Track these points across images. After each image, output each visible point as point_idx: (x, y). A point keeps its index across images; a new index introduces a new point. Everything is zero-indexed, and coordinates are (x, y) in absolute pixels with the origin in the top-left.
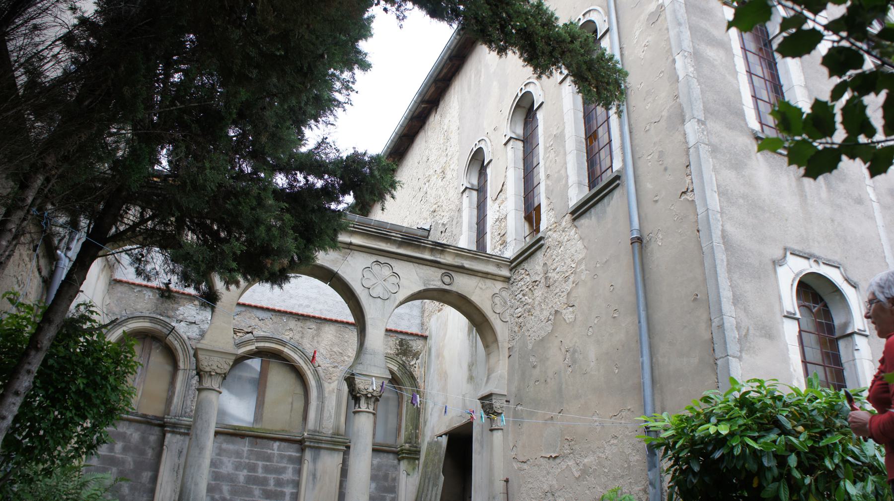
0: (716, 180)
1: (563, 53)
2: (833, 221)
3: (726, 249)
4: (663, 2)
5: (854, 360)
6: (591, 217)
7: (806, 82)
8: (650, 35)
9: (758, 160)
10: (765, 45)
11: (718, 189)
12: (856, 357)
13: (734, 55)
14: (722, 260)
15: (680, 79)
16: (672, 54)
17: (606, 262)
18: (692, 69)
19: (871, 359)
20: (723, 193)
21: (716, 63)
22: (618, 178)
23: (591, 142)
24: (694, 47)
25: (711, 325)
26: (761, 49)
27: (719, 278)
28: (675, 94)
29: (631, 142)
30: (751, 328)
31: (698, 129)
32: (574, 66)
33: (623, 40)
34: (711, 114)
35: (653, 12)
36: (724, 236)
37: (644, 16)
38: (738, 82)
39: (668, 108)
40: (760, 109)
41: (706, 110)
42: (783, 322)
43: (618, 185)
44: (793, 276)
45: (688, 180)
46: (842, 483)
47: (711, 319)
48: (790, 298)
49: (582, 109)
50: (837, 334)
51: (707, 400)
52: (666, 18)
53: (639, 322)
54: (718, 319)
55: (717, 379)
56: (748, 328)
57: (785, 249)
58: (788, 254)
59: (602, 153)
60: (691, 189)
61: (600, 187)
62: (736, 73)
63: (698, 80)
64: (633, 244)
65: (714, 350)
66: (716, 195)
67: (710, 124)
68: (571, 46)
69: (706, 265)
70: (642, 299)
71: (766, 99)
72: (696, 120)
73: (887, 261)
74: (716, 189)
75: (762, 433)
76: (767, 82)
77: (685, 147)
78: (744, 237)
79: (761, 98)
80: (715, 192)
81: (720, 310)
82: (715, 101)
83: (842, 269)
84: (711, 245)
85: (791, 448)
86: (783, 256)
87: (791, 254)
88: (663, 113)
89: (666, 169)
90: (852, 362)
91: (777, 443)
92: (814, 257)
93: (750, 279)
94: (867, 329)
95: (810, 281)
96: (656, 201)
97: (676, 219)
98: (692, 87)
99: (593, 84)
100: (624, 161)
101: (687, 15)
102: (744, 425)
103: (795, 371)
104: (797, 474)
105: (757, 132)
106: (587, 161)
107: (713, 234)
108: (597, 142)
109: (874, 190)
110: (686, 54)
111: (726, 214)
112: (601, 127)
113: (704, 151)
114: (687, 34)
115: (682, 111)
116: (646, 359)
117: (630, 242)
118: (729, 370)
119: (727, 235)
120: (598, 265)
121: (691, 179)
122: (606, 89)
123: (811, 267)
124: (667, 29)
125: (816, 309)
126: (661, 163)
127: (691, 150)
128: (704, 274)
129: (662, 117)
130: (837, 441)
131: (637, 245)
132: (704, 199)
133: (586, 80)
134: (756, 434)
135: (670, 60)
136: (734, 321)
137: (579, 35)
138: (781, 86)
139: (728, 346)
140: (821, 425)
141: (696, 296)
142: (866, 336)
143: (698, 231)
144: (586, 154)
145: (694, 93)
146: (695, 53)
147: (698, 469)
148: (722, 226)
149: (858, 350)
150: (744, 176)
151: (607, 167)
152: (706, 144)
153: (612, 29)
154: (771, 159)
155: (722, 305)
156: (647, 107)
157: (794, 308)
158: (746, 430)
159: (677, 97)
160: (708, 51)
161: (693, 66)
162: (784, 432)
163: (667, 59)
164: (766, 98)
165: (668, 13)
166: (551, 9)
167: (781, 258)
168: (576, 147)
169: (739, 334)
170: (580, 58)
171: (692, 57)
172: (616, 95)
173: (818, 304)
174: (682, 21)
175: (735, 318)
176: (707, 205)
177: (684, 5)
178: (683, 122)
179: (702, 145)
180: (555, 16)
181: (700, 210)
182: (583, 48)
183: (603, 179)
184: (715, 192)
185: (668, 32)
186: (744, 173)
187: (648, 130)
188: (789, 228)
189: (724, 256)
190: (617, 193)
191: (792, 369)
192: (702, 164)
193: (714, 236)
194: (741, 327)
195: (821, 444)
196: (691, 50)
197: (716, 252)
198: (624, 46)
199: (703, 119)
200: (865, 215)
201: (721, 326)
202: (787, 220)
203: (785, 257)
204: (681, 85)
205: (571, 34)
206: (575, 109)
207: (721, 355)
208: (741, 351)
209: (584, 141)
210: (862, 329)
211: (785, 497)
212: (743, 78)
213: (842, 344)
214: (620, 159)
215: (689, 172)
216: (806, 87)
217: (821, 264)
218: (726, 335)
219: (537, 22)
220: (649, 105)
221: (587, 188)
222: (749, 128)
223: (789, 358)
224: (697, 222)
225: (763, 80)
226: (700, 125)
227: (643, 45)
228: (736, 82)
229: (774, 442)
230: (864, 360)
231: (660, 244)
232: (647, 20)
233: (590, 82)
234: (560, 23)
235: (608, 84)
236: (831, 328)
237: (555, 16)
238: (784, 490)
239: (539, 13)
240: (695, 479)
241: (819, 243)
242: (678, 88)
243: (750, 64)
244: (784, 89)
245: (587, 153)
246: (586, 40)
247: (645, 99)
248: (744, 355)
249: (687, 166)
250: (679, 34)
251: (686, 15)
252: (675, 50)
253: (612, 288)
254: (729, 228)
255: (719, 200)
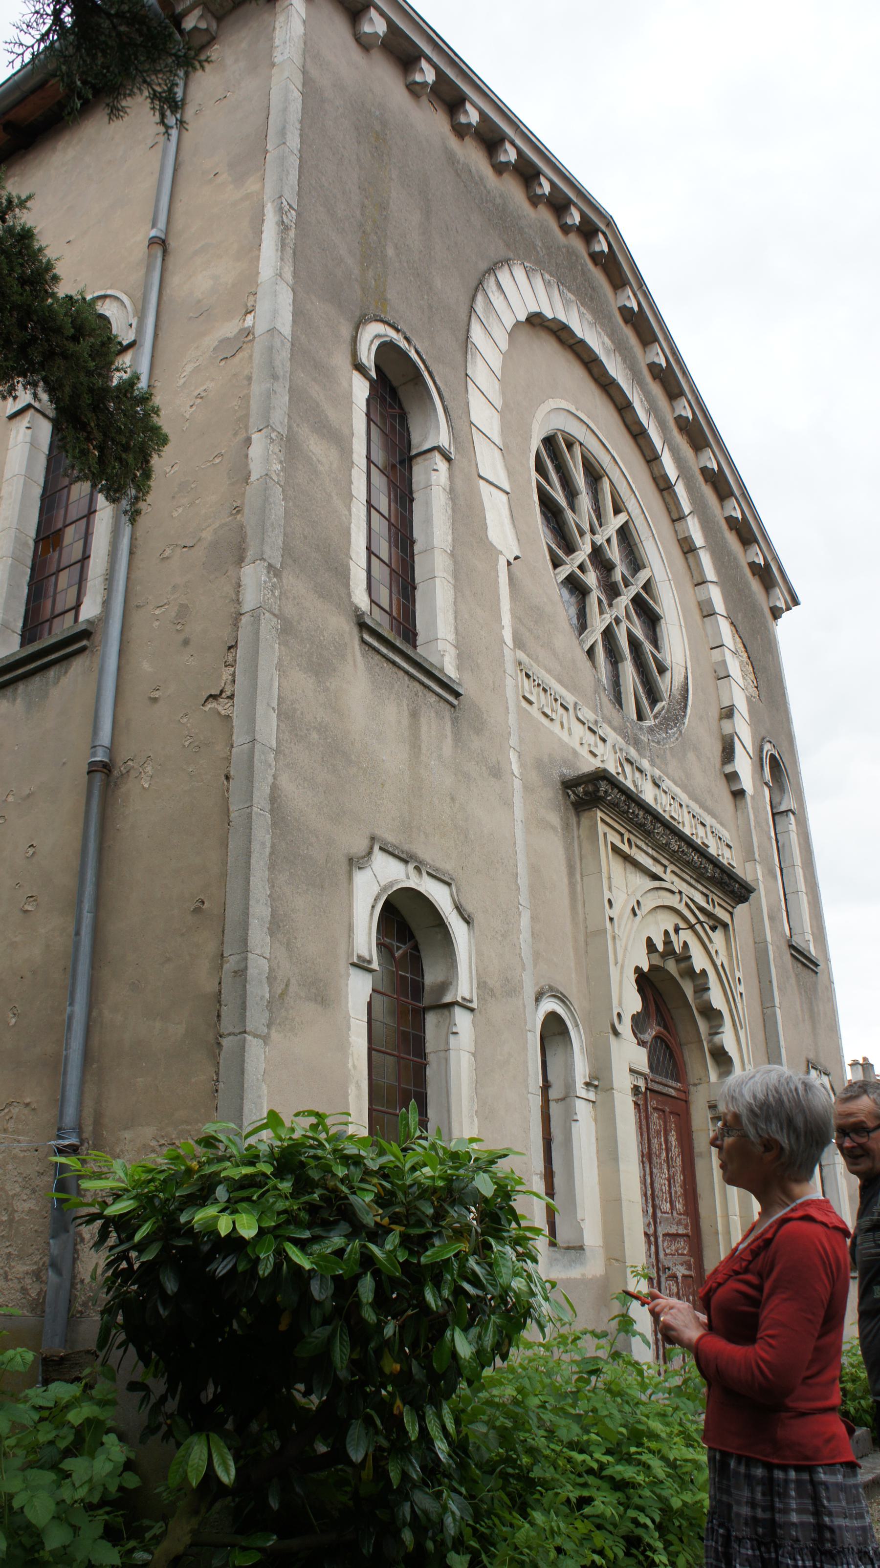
0: (279, 686)
1: (50, 356)
2: (453, 799)
3: (274, 824)
4: (253, 326)
5: (447, 1050)
6: (15, 700)
7: (453, 548)
8: (213, 380)
9: (355, 666)
10: (402, 462)
11: (279, 705)
12: (452, 1046)
13: (353, 463)
14: (263, 844)
15: (253, 477)
16: (246, 428)
17: (29, 796)
18: (279, 467)
19: (473, 1050)
20: (286, 714)
21: (320, 468)
22: (86, 634)
23: (46, 551)
24: (290, 428)
25: (221, 967)
26: (393, 467)
27: (252, 878)
28: (235, 505)
29: (128, 573)
30: (293, 981)
31: (265, 582)
32: (67, 389)
33: (157, 371)
34: (295, 561)
35: (228, 339)
36: (274, 797)
37: (210, 341)
38: (350, 515)
39: (217, 525)
40: (373, 573)
41: (287, 550)
42: (348, 975)
43: (83, 649)
44: (376, 889)
45: (226, 675)
46: (448, 1333)
47: (222, 955)
48: (366, 931)
49: (41, 481)
50: (427, 1001)
51: (209, 1142)
52: (251, 356)
53: (78, 933)
54: (237, 957)
55: (217, 1074)
56: (289, 980)
57: (373, 839)
58: (376, 848)
59: (64, 577)
60: (229, 693)
61: (41, 647)
62: (350, 496)
63: (283, 491)
64: (92, 774)
65: (219, 1016)
66: (274, 716)
67: (289, 579)
68: (71, 347)
69: (230, 847)
70: (89, 889)
71: (385, 558)
72: (266, 564)
73: (519, 881)
74: (275, 704)
75: (318, 1231)
76: (392, 527)
77: (233, 610)
78: (307, 806)
79: (377, 553)
80: (273, 709)
81: (244, 941)
82: (305, 538)
83: (453, 887)
84: (248, 810)
85: (367, 1261)
86: (367, 850)
87: (381, 849)
88: (204, 534)
89: (186, 642)
90: (442, 1054)
91: (345, 1256)
92: (416, 861)
93: (305, 888)
94: (475, 999)
95: (404, 907)
96: (155, 700)
97: (187, 743)
98: (271, 500)
99: (94, 439)
100: (106, 604)
101: (291, 365)
102: (285, 1212)
103: (354, 1067)
104: (370, 1315)
105: (363, 613)
106: (30, 585)
107: (255, 791)
108: (57, 554)
109: (519, 757)
110: (273, 435)
111: (284, 755)
112: (73, 526)
113: (268, 625)
114: (283, 399)
115: (243, 539)
116: (79, 1010)
117: (85, 768)
118: (243, 1061)
119: (280, 796)
120: (11, 799)
121: (233, 675)
122: (120, 460)
123: (408, 878)
124: (249, 379)
125: (400, 952)
126: (178, 627)
127: (244, 619)
128: (224, 863)
129: (199, 540)
130: (451, 1254)
131: (98, 777)
132: (251, 720)
133: (84, 427)
134: (306, 1235)
135: (242, 436)
136: (265, 965)
137: (94, 330)
138: (413, 542)
139: (247, 1014)
140: (426, 1220)
141: (199, 904)
142: (472, 1010)
143: (227, 778)
144: (29, 571)
145: (273, 511)
146: (289, 439)
147: (175, 1290)
148: (275, 777)
149: (456, 1033)
150: (328, 689)
151: (67, 607)
152: (275, 615)
153: (142, 345)
154: (377, 669)
155: (250, 932)
156: (175, 514)
157: (370, 951)
158: (288, 1222)
159: (238, 510)
160: (312, 442)
161: (281, 462)
162: (357, 1229)
163: (235, 434)
164: (385, 556)
165: (258, 348)
166: (50, 253)
167: (364, 854)
168: (13, 553)
169: (270, 992)
170: (83, 378)
171: (283, 443)
172: (135, 475)
173: (405, 944)
174: (281, 373)
175: (269, 960)
176: (254, 731)
177: (289, 345)
178: (240, 560)
179: (267, 614)
180: (54, 271)
181: (239, 738)
182: (93, 360)
183: (54, 631)
184: (273, 709)
185: (250, 384)
186: (328, 684)
187: (167, 558)
188: (385, 802)
189: (268, 837)
190: (78, 665)
191: (350, 1065)
192: (260, 651)
193: (256, 794)
194: (275, 978)
195: (423, 1260)
196: (285, 432)
197: (254, 826)
198: (157, 384)
199: (278, 566)
200: (500, 797)
201: (241, 973)
202: (383, 785)
203: (370, 853)
204: (252, 492)
205: (79, 322)
206: (28, 477)
207: (231, 1030)
208: (269, 1026)
209: (31, 543)
210: (468, 997)
211: (342, 1358)
212: (359, 510)
213: (431, 1019)
214: (99, 600)
215: (231, 659)
216: (452, 555)
217: (424, 874)
218: (248, 992)
219: (11, 270)
220: (180, 510)
221: (17, 639)
222: (352, 603)
223: (349, 1043)
224: (228, 759)
225: (386, 522)
226: (271, 575)
227: (196, 393)
228: (347, 513)
229: (339, 1253)
230: (462, 1052)
231: (146, 785)
232: (214, 349)
233: (89, 433)
234: (62, 290)
235: (126, 448)
236: (417, 988)
237: (54, 271)
238: (341, 1343)
239: (20, 253)
240: (165, 1309)
241: (426, 835)
242: (244, 494)
243: (372, 486)
244: (417, 548)
245: (33, 569)
246: (103, 344)
247: (173, 497)
248: (275, 1035)
249: (230, 648)
250: (269, 395)
251: (288, 364)
252: (254, 421)
253: (31, 851)
254: (285, 781)
255: (278, 726)
